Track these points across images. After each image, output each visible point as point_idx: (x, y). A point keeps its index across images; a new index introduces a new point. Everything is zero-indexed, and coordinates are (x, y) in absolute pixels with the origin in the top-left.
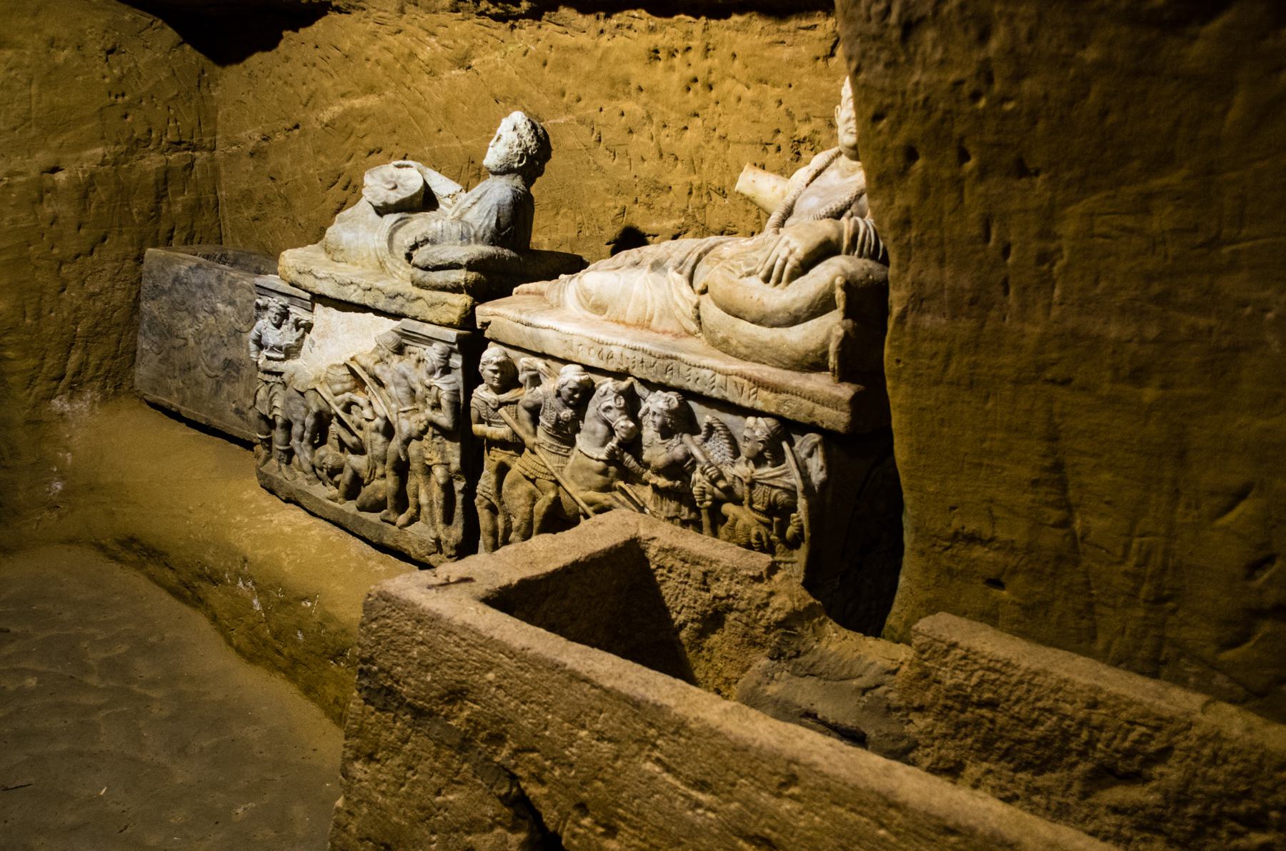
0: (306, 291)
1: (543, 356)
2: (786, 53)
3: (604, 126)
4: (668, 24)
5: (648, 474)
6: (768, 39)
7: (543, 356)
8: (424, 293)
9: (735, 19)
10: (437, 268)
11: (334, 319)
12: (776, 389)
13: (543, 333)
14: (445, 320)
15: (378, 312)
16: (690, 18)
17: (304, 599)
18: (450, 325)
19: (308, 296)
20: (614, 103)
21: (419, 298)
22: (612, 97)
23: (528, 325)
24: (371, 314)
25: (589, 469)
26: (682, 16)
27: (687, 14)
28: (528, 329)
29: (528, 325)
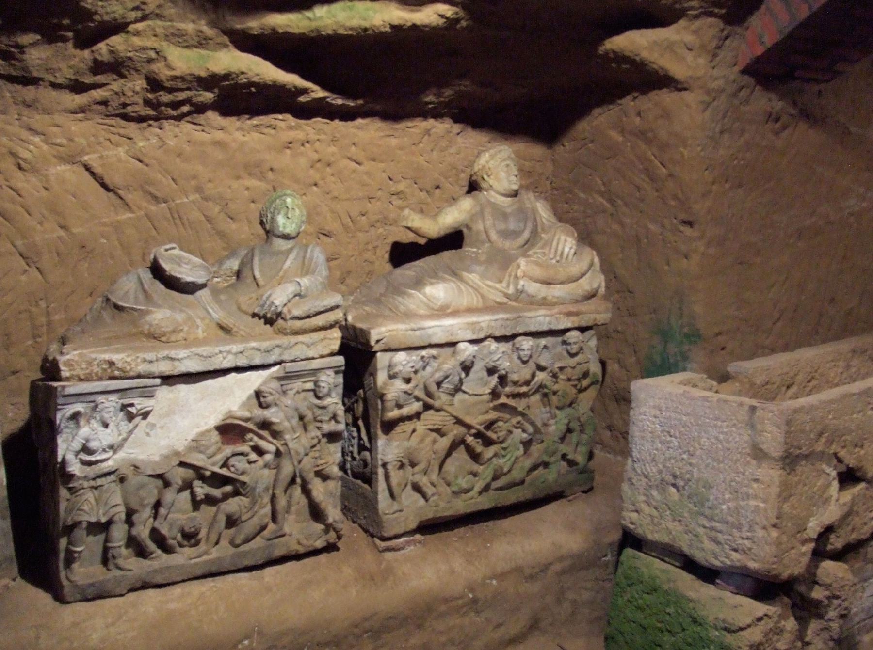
0: (154, 378)
1: (431, 346)
2: (394, 142)
3: (231, 200)
4: (307, 125)
5: (255, 428)
6: (382, 134)
7: (431, 346)
8: (300, 338)
9: (359, 121)
10: (309, 317)
11: (182, 394)
12: (576, 314)
13: (430, 331)
14: (327, 351)
15: (238, 369)
16: (328, 121)
17: (240, 642)
18: (332, 354)
19: (158, 381)
20: (241, 181)
21: (296, 343)
22: (238, 178)
23: (419, 329)
24: (233, 374)
25: (481, 402)
26: (319, 119)
27: (323, 118)
28: (418, 333)
29: (419, 329)
